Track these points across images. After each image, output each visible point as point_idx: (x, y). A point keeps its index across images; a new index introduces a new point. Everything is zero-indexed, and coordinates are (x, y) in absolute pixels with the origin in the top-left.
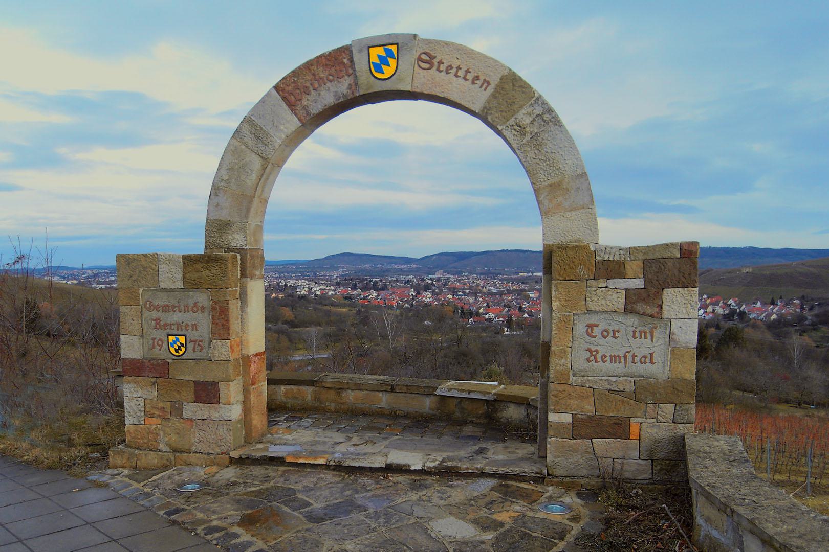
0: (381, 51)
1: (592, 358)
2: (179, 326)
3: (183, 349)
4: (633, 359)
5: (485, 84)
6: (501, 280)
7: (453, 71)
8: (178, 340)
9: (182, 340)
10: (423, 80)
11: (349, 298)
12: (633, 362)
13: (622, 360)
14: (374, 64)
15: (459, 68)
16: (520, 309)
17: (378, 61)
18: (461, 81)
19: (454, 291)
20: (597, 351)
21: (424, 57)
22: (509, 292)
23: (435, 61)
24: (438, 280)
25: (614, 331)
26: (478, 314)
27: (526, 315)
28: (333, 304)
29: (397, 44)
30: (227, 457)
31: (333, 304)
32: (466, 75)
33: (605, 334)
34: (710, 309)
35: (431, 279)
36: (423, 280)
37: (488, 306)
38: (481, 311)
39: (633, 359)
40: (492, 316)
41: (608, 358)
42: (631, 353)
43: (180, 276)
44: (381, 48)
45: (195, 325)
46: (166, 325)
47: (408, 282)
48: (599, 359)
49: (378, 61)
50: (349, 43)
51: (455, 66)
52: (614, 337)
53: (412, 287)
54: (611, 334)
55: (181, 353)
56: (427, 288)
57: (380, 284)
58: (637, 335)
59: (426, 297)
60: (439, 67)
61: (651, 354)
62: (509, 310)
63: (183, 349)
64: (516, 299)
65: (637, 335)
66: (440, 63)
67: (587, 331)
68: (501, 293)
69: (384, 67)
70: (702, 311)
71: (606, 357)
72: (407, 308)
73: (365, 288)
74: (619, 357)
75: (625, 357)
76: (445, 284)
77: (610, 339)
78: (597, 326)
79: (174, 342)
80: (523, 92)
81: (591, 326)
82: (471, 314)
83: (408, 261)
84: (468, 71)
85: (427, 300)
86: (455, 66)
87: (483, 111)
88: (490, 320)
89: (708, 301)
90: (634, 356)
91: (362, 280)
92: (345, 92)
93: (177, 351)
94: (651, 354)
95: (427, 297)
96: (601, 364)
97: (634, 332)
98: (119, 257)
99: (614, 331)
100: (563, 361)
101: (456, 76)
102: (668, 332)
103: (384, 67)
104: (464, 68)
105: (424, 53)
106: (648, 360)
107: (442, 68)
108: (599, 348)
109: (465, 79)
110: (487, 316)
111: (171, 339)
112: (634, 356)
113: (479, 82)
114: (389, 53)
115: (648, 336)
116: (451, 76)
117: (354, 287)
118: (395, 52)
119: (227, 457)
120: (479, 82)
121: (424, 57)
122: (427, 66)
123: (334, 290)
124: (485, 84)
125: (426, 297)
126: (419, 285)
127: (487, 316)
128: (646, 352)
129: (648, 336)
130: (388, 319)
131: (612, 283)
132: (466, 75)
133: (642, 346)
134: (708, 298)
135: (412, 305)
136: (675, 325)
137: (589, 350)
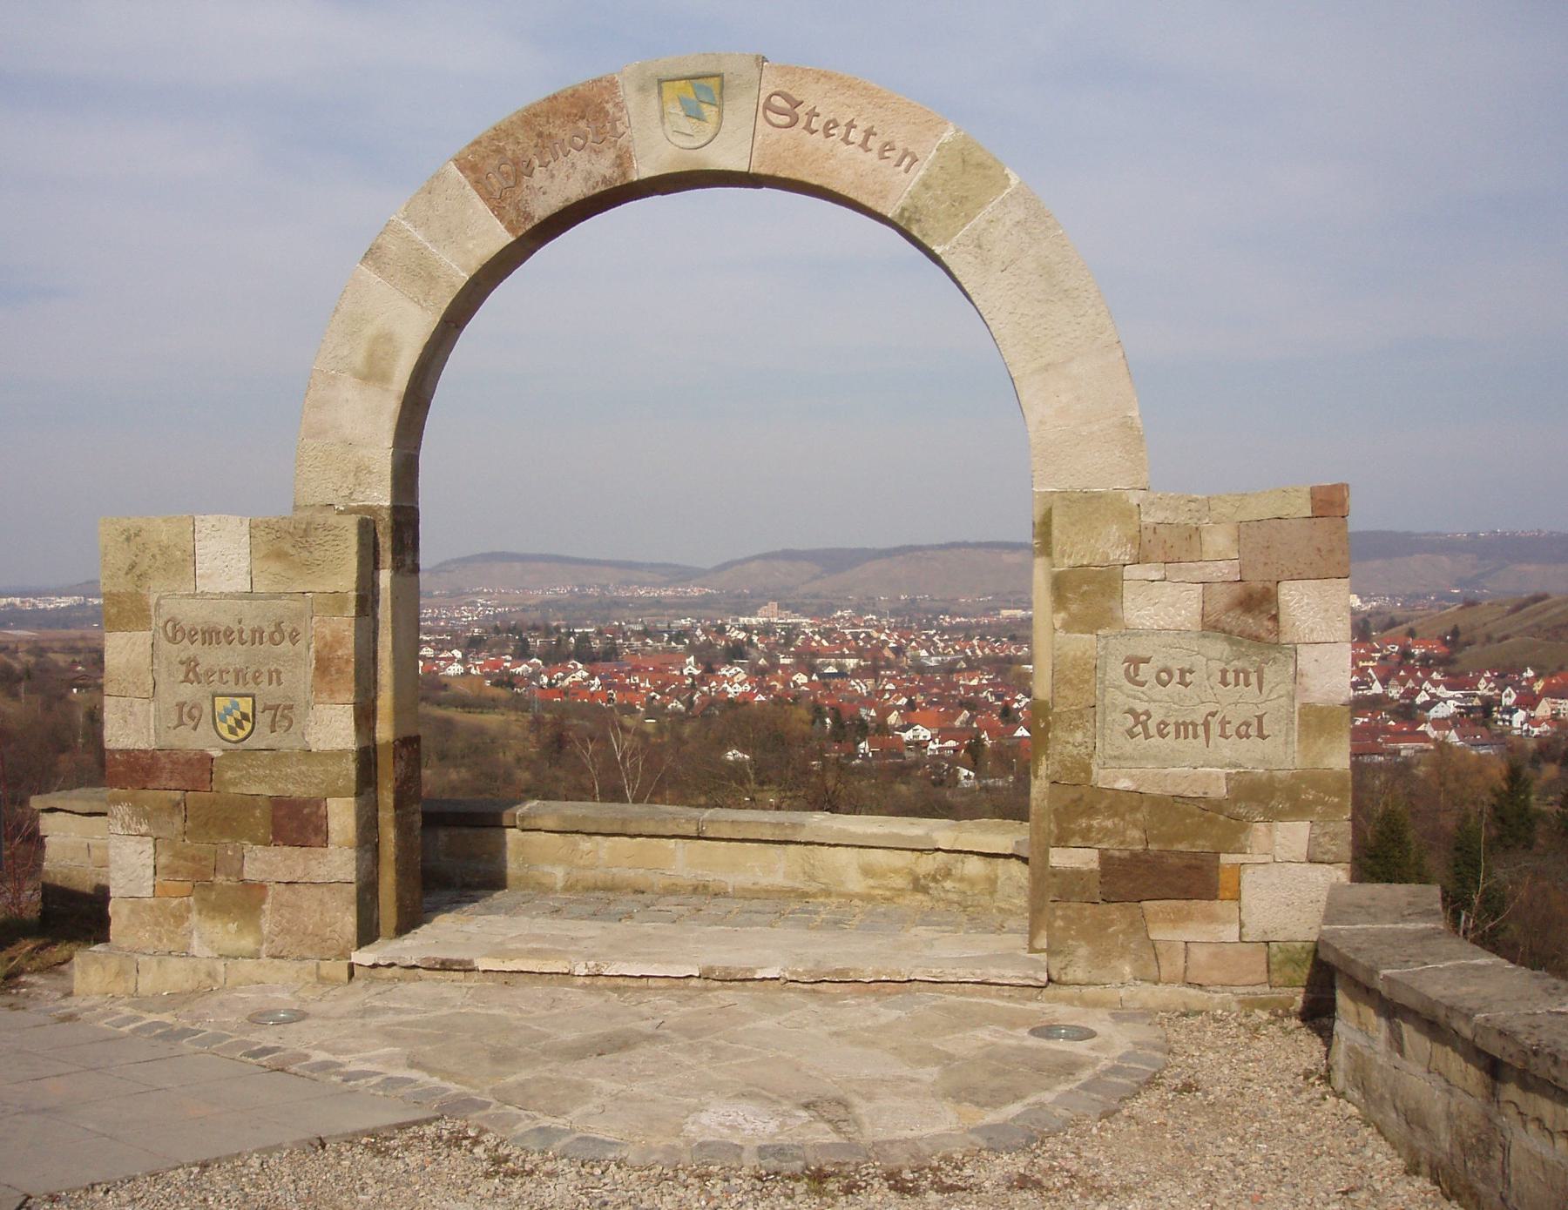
1: (1139, 728)
3: (248, 726)
4: (1223, 729)
5: (907, 160)
6: (953, 629)
8: (236, 706)
9: (245, 705)
11: (508, 681)
12: (1223, 735)
13: (1201, 730)
15: (851, 125)
16: (1007, 713)
19: (807, 660)
20: (1148, 714)
21: (778, 102)
22: (973, 666)
24: (766, 630)
25: (1183, 672)
26: (882, 728)
27: (1022, 732)
28: (465, 704)
31: (465, 704)
32: (866, 139)
33: (1164, 676)
35: (745, 628)
36: (721, 630)
37: (911, 705)
38: (893, 719)
39: (1223, 729)
40: (923, 733)
41: (1171, 728)
42: (1219, 717)
46: (210, 673)
47: (678, 636)
48: (1153, 730)
51: (843, 122)
52: (1182, 682)
53: (692, 649)
54: (1176, 678)
55: (242, 734)
56: (736, 652)
57: (596, 644)
58: (1230, 677)
59: (731, 681)
61: (1260, 718)
62: (972, 718)
63: (248, 726)
64: (991, 684)
65: (1230, 677)
66: (813, 114)
67: (1127, 670)
68: (949, 669)
71: (1167, 725)
72: (676, 712)
73: (555, 656)
74: (1195, 725)
75: (1206, 725)
76: (789, 641)
78: (1147, 661)
79: (229, 712)
80: (985, 177)
81: (1135, 661)
82: (862, 729)
83: (684, 575)
84: (869, 133)
85: (733, 691)
86: (843, 122)
87: (901, 215)
88: (920, 745)
89: (1538, 686)
90: (1224, 723)
91: (548, 631)
92: (608, 173)
93: (232, 731)
94: (1260, 718)
95: (734, 682)
96: (1156, 740)
97: (1224, 672)
98: (494, 881)
99: (1183, 672)
100: (1079, 736)
102: (1291, 670)
104: (862, 125)
105: (776, 94)
106: (1253, 731)
107: (816, 124)
108: (1152, 707)
109: (864, 145)
110: (908, 736)
111: (221, 703)
112: (1224, 723)
113: (894, 155)
115: (1253, 679)
117: (523, 654)
118: (716, 92)
120: (894, 155)
121: (778, 102)
122: (785, 120)
123: (464, 661)
124: (907, 160)
125: (731, 681)
126: (709, 645)
127: (908, 736)
128: (1248, 712)
129: (1253, 679)
130: (620, 745)
132: (866, 139)
133: (1241, 703)
134: (1537, 678)
135: (690, 703)
136: (1306, 657)
137: (1131, 711)
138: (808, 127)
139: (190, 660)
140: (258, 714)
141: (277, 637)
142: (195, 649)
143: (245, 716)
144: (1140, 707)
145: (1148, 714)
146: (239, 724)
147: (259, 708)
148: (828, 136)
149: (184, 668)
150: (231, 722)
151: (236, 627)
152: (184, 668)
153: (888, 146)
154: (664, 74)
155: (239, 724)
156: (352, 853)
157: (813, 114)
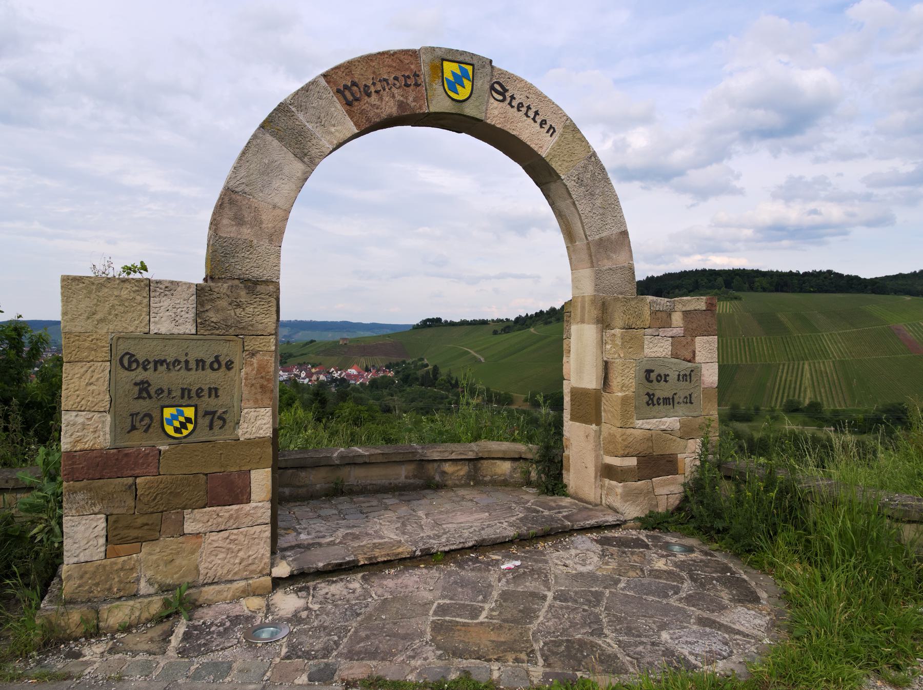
0: (455, 67)
2: (185, 392)
3: (190, 427)
7: (524, 109)
8: (181, 413)
9: (190, 412)
10: (496, 113)
14: (468, 78)
17: (451, 78)
18: (530, 121)
21: (497, 87)
23: (508, 95)
29: (472, 65)
30: (269, 578)
34: (314, 378)
43: (191, 315)
44: (456, 65)
45: (216, 389)
48: (655, 402)
49: (451, 78)
50: (417, 47)
51: (525, 105)
55: (185, 432)
60: (511, 101)
63: (190, 427)
69: (459, 88)
70: (307, 380)
77: (662, 383)
79: (174, 417)
86: (525, 105)
93: (177, 430)
94: (690, 395)
98: (70, 284)
101: (526, 115)
103: (459, 88)
104: (534, 110)
114: (465, 73)
116: (522, 113)
119: (269, 578)
121: (497, 87)
122: (501, 98)
131: (662, 332)
138: (510, 104)
139: (142, 382)
140: (200, 420)
141: (216, 366)
142: (148, 375)
143: (188, 420)
144: (651, 392)
145: (653, 395)
146: (183, 425)
147: (200, 413)
148: (519, 110)
149: (137, 388)
150: (177, 424)
151: (183, 359)
152: (137, 388)
153: (543, 122)
154: (445, 57)
155: (183, 425)
156: (332, 340)
157: (512, 98)
